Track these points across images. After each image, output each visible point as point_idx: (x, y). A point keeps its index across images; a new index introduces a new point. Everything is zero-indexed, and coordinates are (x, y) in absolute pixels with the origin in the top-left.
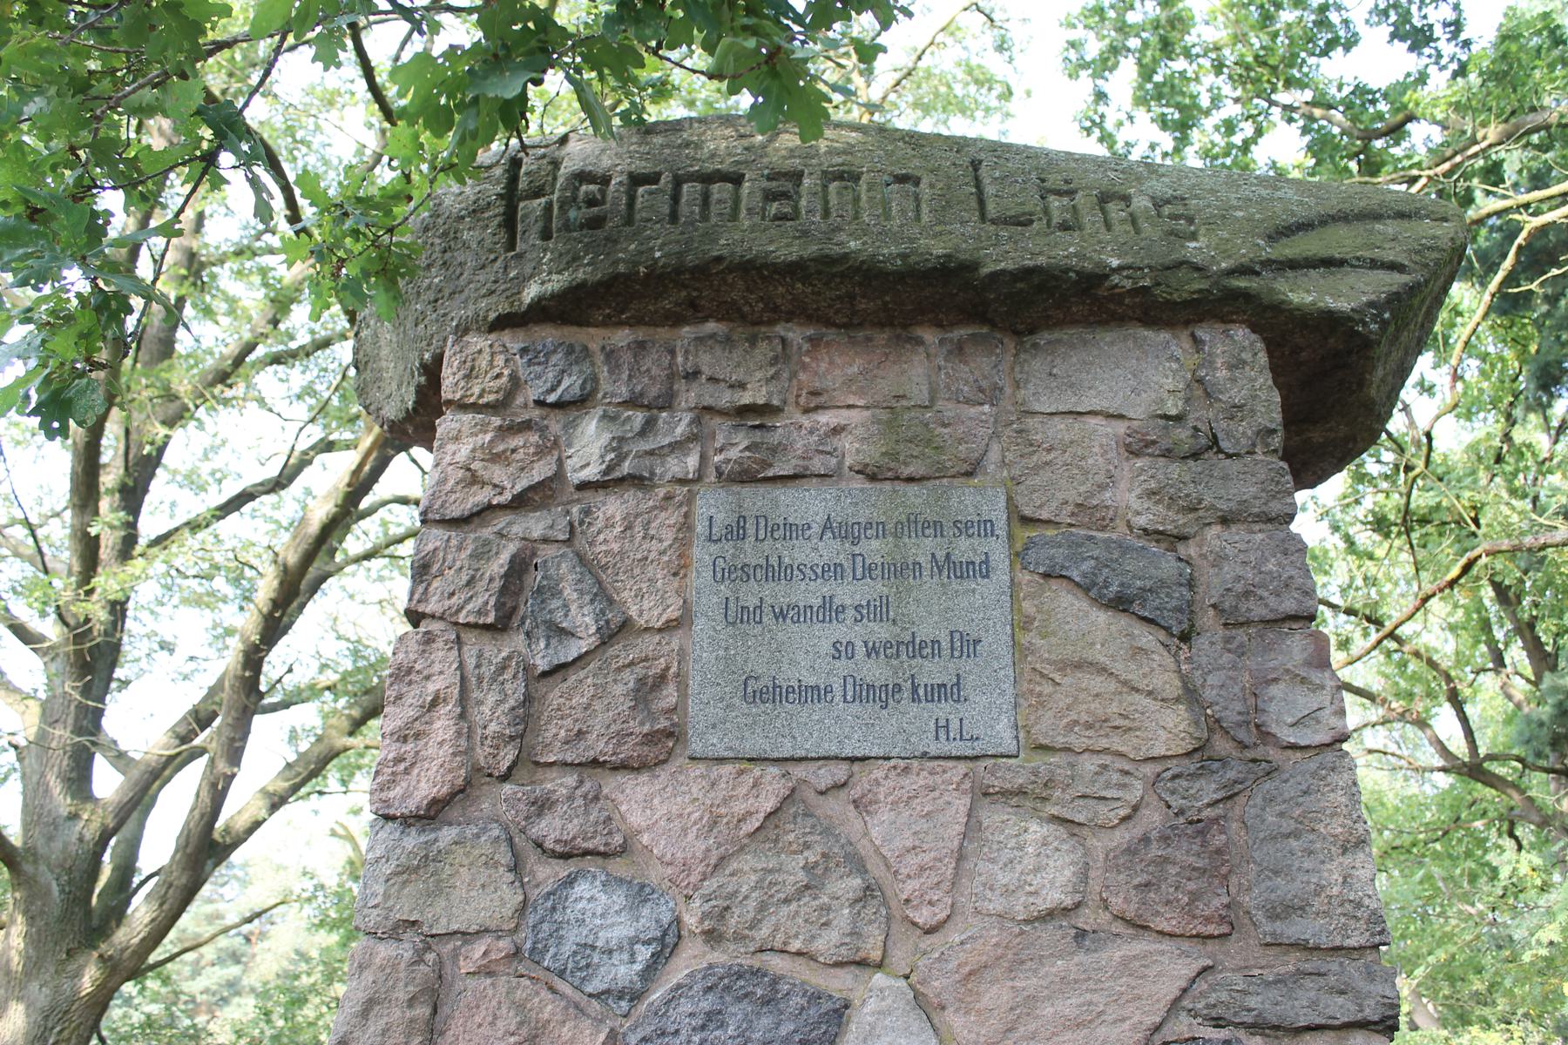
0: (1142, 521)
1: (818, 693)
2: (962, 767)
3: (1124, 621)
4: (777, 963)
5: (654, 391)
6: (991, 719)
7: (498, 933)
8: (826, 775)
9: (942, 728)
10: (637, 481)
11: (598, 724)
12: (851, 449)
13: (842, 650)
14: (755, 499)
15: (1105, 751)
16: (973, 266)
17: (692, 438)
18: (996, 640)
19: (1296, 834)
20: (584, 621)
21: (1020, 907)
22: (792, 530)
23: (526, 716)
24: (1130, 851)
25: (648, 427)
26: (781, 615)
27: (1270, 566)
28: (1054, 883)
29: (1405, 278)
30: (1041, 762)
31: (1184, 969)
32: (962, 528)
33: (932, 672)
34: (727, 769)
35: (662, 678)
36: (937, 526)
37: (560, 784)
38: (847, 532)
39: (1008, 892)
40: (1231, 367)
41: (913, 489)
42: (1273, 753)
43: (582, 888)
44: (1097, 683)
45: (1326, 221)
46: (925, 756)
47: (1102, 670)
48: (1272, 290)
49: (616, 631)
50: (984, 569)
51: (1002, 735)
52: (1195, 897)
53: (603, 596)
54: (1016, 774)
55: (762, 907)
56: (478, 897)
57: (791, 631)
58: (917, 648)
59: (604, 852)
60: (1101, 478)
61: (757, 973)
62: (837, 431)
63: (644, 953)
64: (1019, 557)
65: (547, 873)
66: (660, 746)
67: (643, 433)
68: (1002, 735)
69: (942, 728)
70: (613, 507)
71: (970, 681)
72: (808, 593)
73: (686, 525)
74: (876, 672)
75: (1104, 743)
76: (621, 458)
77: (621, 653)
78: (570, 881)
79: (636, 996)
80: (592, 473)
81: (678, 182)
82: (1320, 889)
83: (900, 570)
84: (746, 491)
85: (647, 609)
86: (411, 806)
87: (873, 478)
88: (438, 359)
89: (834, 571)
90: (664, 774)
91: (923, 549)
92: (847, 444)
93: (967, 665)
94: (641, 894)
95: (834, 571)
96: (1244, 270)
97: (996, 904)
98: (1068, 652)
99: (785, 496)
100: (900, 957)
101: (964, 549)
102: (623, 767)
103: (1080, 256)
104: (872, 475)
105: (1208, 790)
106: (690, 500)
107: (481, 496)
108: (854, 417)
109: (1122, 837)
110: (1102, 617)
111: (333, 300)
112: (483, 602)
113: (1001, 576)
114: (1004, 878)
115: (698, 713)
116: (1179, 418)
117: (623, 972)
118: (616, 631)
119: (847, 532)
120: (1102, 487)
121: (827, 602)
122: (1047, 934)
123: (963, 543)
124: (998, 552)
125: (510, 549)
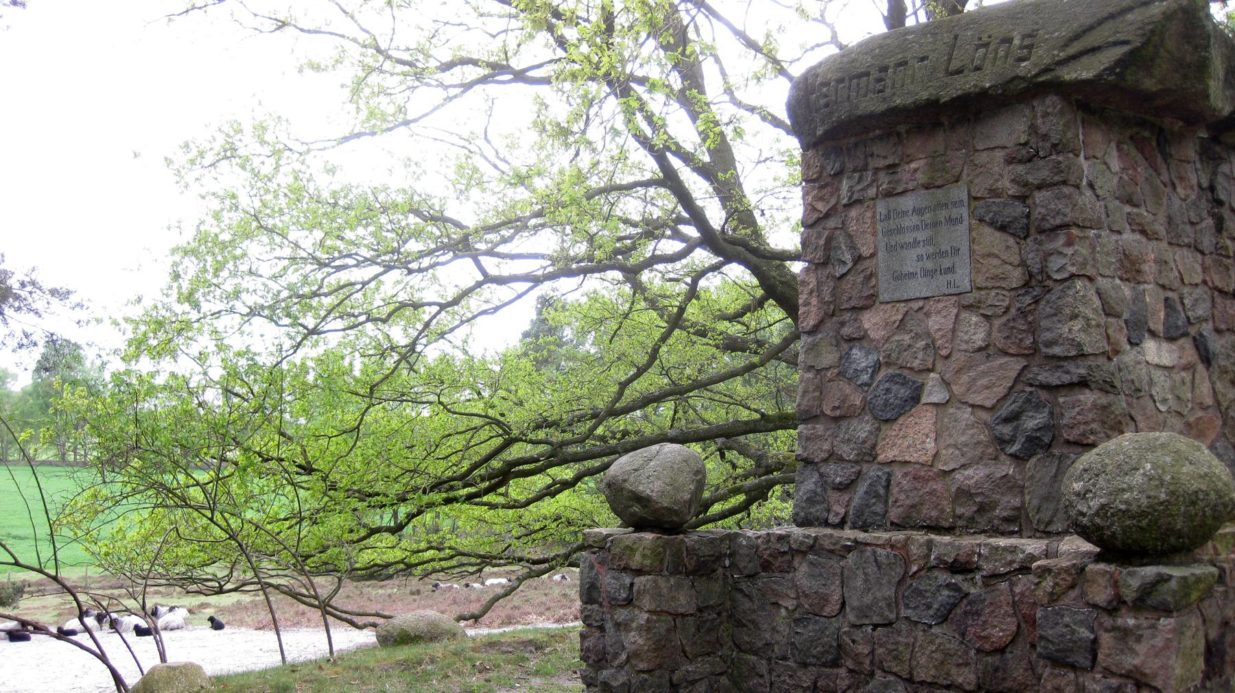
0: (1010, 193)
1: (913, 275)
2: (955, 298)
3: (1005, 236)
4: (906, 372)
5: (861, 164)
7: (835, 367)
8: (916, 305)
9: (949, 283)
12: (921, 178)
13: (920, 258)
14: (893, 202)
15: (998, 287)
16: (937, 101)
17: (873, 181)
18: (965, 249)
19: (1055, 315)
20: (848, 257)
21: (970, 347)
22: (905, 213)
24: (1005, 325)
25: (861, 178)
26: (902, 247)
27: (1052, 206)
28: (979, 338)
29: (1126, 48)
30: (976, 294)
32: (955, 204)
33: (946, 263)
34: (889, 306)
35: (871, 275)
36: (946, 205)
38: (918, 211)
39: (967, 342)
40: (1043, 117)
41: (939, 191)
42: (1049, 283)
43: (854, 351)
44: (995, 262)
45: (1100, 22)
46: (945, 295)
47: (997, 256)
48: (1058, 77)
49: (858, 259)
50: (959, 221)
51: (966, 285)
52: (1021, 340)
53: (852, 247)
54: (969, 299)
55: (899, 353)
57: (905, 253)
60: (997, 177)
61: (899, 375)
62: (916, 170)
63: (870, 371)
64: (972, 214)
67: (859, 182)
68: (966, 285)
69: (949, 283)
71: (957, 265)
72: (908, 238)
73: (874, 217)
74: (929, 265)
75: (998, 284)
76: (853, 194)
77: (860, 267)
78: (851, 349)
79: (869, 385)
81: (851, 80)
82: (1060, 336)
83: (935, 224)
84: (889, 200)
85: (866, 251)
86: (808, 328)
87: (927, 188)
89: (916, 228)
90: (873, 309)
91: (943, 214)
92: (919, 175)
93: (956, 259)
95: (916, 228)
96: (1047, 70)
97: (964, 347)
98: (985, 251)
99: (901, 200)
100: (939, 366)
101: (955, 212)
103: (975, 86)
104: (927, 187)
105: (1028, 300)
106: (874, 206)
108: (922, 162)
109: (1004, 319)
110: (998, 234)
113: (966, 223)
114: (966, 338)
115: (882, 286)
116: (1025, 144)
117: (865, 378)
118: (858, 259)
120: (997, 181)
121: (915, 240)
122: (978, 356)
123: (955, 210)
124: (964, 212)
125: (826, 233)
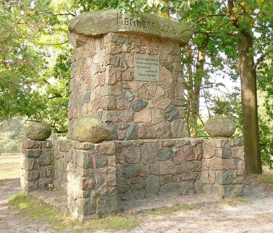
4: (144, 100)
6: (157, 78)
8: (146, 82)
10: (129, 52)
11: (127, 76)
23: (121, 75)
31: (171, 101)
33: (154, 74)
37: (124, 82)
38: (147, 60)
49: (128, 68)
53: (127, 64)
56: (118, 92)
58: (153, 72)
59: (128, 89)
65: (124, 91)
66: (132, 79)
70: (127, 55)
80: (125, 51)
88: (106, 34)
94: (132, 93)
102: (130, 81)
107: (115, 52)
111: (80, 5)
112: (117, 64)
115: (135, 77)
117: (131, 99)
119: (147, 60)
